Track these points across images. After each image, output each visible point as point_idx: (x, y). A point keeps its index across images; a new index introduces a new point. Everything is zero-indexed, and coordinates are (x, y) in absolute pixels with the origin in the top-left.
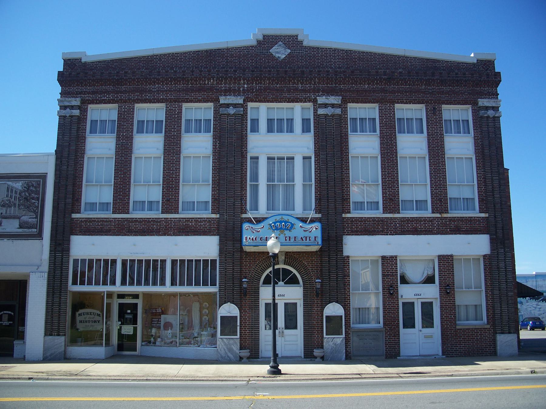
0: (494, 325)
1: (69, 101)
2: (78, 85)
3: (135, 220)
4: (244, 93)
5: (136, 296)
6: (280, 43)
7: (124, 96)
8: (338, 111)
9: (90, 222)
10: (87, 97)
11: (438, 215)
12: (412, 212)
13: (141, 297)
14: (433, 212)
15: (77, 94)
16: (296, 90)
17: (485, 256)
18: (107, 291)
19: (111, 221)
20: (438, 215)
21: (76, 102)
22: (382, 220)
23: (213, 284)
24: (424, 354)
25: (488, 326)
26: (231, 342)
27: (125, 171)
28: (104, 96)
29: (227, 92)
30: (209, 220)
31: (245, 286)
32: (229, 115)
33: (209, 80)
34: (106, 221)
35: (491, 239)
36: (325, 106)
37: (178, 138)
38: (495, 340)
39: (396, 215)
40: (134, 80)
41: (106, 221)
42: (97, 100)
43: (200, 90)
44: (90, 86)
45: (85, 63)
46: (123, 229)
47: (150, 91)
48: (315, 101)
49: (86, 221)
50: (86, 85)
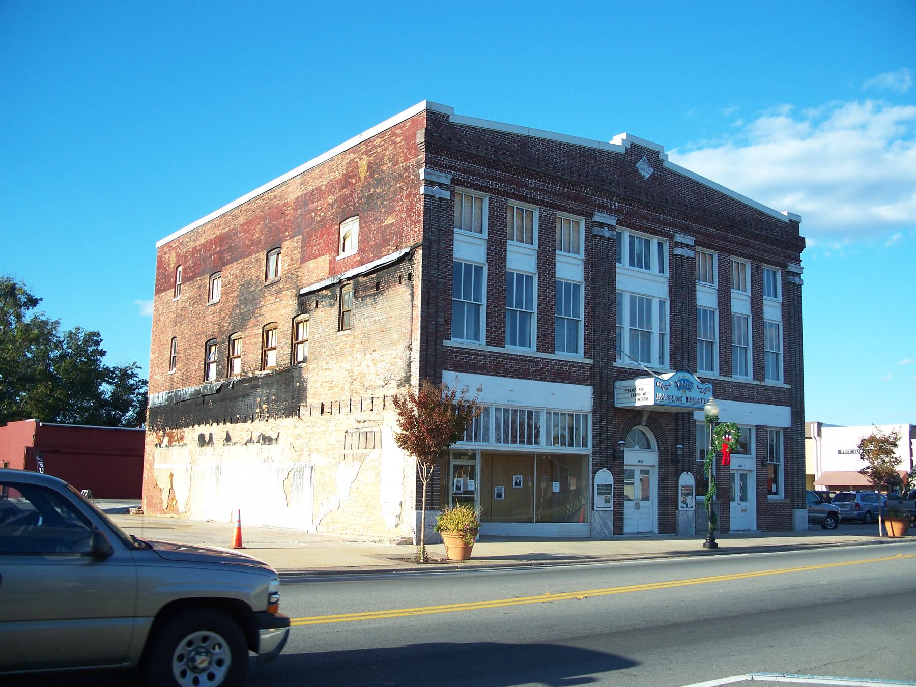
0: (793, 501)
1: (438, 177)
2: (447, 155)
3: (512, 358)
4: (616, 212)
5: (473, 456)
6: (645, 158)
7: (500, 186)
8: (446, 195)
9: (462, 353)
10: (460, 176)
11: (758, 383)
12: (562, 353)
13: (479, 457)
14: (538, 350)
15: (446, 168)
16: (659, 222)
17: (785, 429)
18: (481, 450)
19: (485, 356)
20: (758, 383)
21: (446, 179)
22: (532, 360)
23: (585, 445)
24: (643, 530)
25: (788, 501)
26: (607, 515)
27: (500, 289)
28: (478, 180)
29: (603, 208)
30: (583, 366)
31: (680, 453)
32: (603, 237)
33: (586, 187)
34: (481, 355)
35: (792, 412)
36: (682, 245)
37: (504, 245)
38: (791, 515)
39: (730, 379)
40: (512, 166)
41: (481, 355)
42: (468, 183)
43: (576, 198)
44: (460, 160)
45: (453, 124)
46: (499, 368)
47: (526, 187)
48: (672, 237)
49: (457, 352)
50: (456, 158)
